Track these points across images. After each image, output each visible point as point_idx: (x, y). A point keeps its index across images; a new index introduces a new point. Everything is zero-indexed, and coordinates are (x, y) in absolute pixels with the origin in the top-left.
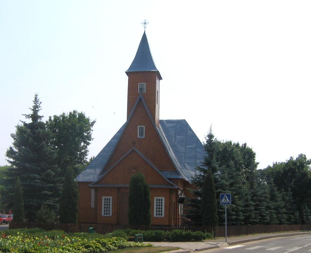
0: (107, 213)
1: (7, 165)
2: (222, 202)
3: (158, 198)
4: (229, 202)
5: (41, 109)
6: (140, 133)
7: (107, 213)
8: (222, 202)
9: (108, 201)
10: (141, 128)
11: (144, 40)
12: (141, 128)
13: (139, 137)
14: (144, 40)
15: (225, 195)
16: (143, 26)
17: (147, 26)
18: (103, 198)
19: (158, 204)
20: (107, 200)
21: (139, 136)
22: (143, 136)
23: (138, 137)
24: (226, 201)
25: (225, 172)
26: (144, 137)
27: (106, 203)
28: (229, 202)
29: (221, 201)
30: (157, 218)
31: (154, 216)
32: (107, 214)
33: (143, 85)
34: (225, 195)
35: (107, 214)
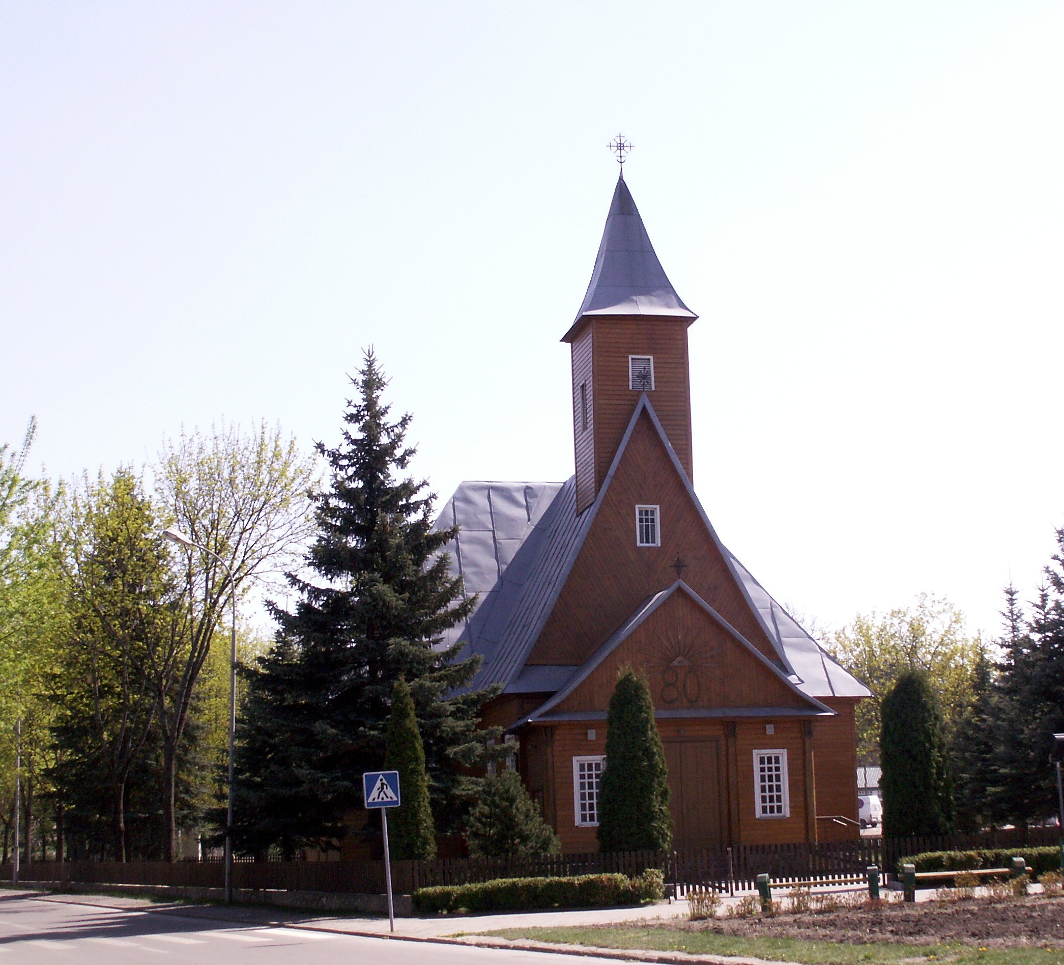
0: (772, 808)
1: (862, 629)
2: (370, 800)
3: (767, 752)
4: (395, 799)
5: (350, 403)
6: (641, 527)
7: (772, 808)
8: (370, 800)
9: (773, 765)
10: (647, 514)
11: (623, 203)
12: (647, 514)
13: (642, 545)
14: (623, 203)
15: (381, 777)
16: (614, 154)
17: (627, 154)
18: (757, 754)
19: (767, 773)
20: (770, 761)
21: (642, 542)
22: (653, 542)
23: (639, 544)
24: (382, 794)
25: (912, 668)
26: (658, 542)
27: (767, 773)
28: (395, 799)
29: (368, 797)
30: (766, 821)
31: (757, 816)
32: (772, 811)
33: (640, 363)
34: (381, 777)
35: (772, 811)
